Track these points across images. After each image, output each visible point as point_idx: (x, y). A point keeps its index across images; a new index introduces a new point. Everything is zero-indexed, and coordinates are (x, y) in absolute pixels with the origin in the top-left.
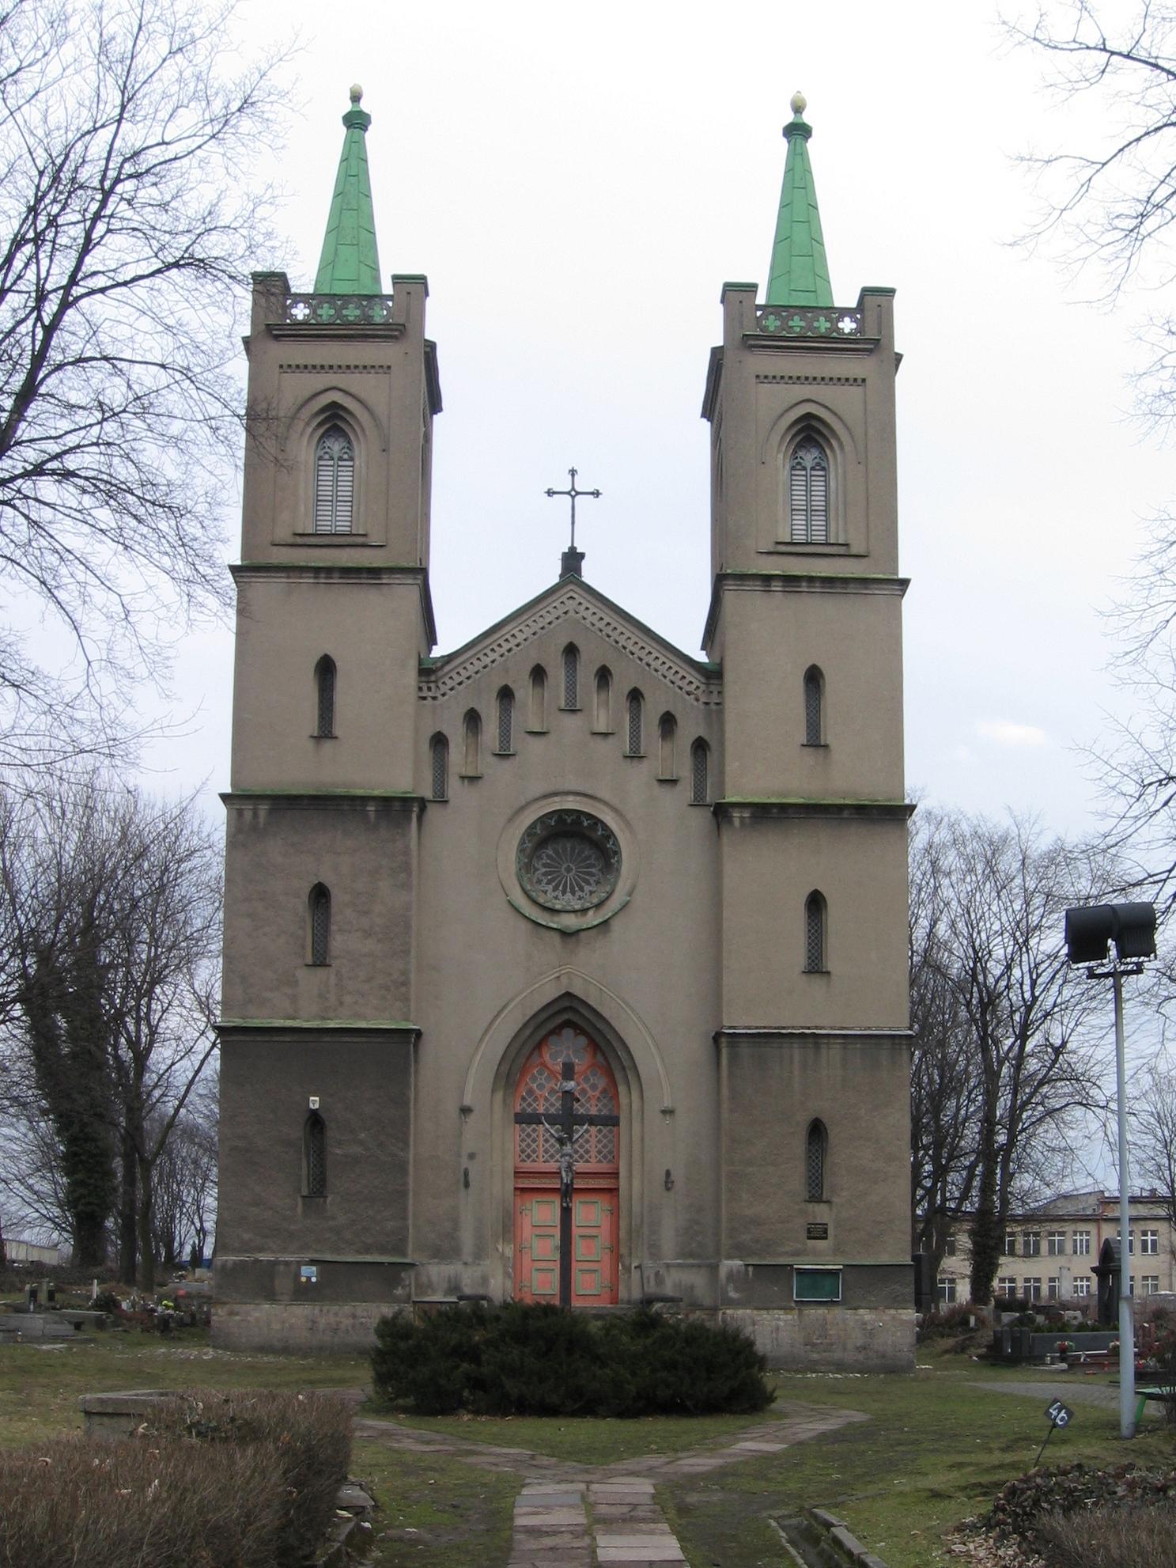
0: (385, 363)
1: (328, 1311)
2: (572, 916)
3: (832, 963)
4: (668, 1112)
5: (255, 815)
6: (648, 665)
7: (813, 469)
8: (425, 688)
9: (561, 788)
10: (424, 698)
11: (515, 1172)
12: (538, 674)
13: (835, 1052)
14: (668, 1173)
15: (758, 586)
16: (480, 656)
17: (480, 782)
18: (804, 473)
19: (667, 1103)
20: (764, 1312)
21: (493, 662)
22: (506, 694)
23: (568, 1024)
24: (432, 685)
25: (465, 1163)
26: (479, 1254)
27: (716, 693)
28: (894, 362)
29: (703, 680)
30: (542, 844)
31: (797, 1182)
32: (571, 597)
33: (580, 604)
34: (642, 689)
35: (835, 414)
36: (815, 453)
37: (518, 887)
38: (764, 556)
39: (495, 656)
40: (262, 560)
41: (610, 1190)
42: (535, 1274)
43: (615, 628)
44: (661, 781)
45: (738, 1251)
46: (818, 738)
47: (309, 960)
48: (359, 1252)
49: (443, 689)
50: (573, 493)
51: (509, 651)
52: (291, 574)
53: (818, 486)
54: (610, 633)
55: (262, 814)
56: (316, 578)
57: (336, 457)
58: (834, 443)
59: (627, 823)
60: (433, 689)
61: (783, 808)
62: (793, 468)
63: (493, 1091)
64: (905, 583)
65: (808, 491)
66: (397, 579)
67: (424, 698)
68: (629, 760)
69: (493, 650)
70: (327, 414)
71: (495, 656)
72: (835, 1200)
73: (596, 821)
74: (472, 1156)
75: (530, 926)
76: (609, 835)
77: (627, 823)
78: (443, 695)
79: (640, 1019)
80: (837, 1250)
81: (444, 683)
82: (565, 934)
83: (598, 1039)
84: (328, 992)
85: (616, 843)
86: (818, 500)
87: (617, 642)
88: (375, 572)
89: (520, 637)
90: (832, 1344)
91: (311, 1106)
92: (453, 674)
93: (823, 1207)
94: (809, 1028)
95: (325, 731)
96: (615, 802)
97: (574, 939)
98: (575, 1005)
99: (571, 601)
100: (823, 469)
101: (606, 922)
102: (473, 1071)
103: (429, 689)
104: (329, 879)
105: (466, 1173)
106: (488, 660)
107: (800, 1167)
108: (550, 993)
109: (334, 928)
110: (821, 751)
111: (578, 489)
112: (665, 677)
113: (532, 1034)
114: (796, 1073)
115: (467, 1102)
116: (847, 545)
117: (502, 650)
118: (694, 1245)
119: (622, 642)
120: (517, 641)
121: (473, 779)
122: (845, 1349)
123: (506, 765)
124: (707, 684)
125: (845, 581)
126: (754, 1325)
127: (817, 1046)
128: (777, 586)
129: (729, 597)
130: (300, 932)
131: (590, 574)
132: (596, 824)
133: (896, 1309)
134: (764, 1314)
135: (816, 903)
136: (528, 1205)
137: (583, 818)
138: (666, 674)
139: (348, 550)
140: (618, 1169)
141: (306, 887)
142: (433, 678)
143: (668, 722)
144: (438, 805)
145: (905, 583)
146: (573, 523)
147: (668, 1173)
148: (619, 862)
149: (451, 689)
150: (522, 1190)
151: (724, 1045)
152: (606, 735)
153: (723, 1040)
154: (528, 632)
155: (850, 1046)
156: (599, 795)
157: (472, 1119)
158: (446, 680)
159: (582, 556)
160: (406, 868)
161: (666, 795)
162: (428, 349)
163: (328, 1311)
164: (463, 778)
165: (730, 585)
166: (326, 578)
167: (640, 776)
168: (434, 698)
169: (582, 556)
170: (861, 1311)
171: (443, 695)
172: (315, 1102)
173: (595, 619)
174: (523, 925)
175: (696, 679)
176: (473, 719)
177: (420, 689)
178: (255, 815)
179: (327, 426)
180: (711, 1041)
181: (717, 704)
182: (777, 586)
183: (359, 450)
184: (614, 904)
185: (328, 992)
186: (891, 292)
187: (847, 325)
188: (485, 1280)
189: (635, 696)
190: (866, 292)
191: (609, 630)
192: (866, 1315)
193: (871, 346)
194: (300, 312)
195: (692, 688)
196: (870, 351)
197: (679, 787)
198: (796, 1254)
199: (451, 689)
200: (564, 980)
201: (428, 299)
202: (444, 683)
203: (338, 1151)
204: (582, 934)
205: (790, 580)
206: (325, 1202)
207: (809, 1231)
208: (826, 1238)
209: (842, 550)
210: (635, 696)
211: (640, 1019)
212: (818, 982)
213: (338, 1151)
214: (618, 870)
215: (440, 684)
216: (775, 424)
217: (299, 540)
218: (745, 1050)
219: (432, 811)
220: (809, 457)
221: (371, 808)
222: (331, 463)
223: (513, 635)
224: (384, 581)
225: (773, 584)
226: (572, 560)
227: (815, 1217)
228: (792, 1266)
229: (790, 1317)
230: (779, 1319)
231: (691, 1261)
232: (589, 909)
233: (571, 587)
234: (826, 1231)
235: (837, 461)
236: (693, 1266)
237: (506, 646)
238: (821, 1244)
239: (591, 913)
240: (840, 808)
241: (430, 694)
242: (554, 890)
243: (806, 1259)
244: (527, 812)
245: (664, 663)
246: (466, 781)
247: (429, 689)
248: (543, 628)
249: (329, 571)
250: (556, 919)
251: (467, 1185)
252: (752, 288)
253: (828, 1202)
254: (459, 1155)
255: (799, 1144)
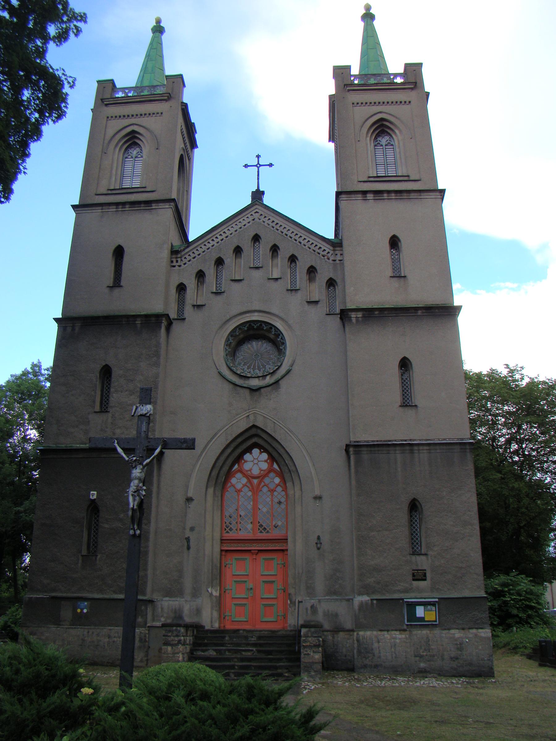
0: (160, 112)
1: (93, 633)
2: (257, 380)
3: (418, 399)
4: (318, 498)
5: (73, 329)
6: (300, 243)
7: (386, 145)
8: (175, 261)
9: (250, 309)
10: (174, 266)
11: (221, 540)
12: (238, 251)
13: (424, 455)
14: (319, 538)
15: (360, 196)
16: (206, 243)
17: (204, 308)
18: (381, 147)
19: (317, 493)
20: (386, 633)
21: (213, 246)
22: (219, 262)
23: (256, 445)
24: (179, 260)
25: (188, 534)
26: (196, 594)
27: (339, 255)
28: (425, 96)
29: (331, 248)
30: (241, 343)
31: (404, 542)
32: (257, 212)
33: (261, 215)
34: (296, 255)
35: (396, 118)
36: (387, 138)
37: (225, 366)
38: (362, 183)
39: (214, 243)
40: (90, 202)
41: (283, 550)
42: (233, 607)
43: (281, 226)
44: (308, 302)
45: (366, 589)
46: (400, 271)
47: (97, 408)
48: (115, 592)
49: (185, 261)
50: (258, 166)
51: (222, 240)
52: (104, 207)
53: (390, 153)
54: (278, 228)
55: (77, 329)
56: (116, 208)
57: (134, 156)
58: (397, 131)
59: (289, 326)
60: (179, 261)
61: (382, 310)
62: (375, 146)
63: (207, 488)
64: (443, 192)
65: (385, 156)
66: (161, 205)
67: (174, 266)
68: (290, 292)
69: (213, 240)
70: (130, 143)
71: (214, 243)
72: (430, 553)
73: (272, 326)
74: (192, 529)
75: (231, 386)
76: (278, 333)
77: (289, 326)
78: (185, 264)
79: (299, 440)
80: (433, 588)
81: (185, 258)
82: (254, 391)
83: (274, 454)
84: (107, 428)
85: (283, 338)
86: (391, 159)
87: (282, 233)
88: (148, 203)
89: (228, 233)
90: (434, 656)
91: (91, 497)
92: (191, 253)
93: (423, 558)
94: (406, 441)
95: (117, 283)
96: (281, 315)
97: (257, 393)
98: (259, 432)
99: (257, 214)
100: (392, 145)
101: (277, 382)
102: (194, 475)
103: (177, 261)
104: (111, 362)
105: (188, 539)
106: (210, 245)
107: (405, 531)
108: (243, 426)
109: (112, 390)
110: (402, 279)
111: (260, 168)
112: (310, 248)
113: (233, 451)
114: (399, 470)
115: (190, 495)
116: (408, 176)
117: (218, 240)
118: (337, 586)
119: (285, 231)
120: (226, 235)
121: (199, 307)
122: (443, 659)
123: (219, 298)
124: (334, 250)
125: (409, 192)
126: (379, 642)
127: (412, 452)
128: (370, 196)
129: (342, 204)
130: (93, 393)
131: (267, 200)
132: (271, 328)
133: (477, 628)
134: (386, 635)
135: (405, 364)
136: (230, 562)
137: (263, 325)
138: (310, 247)
139: (135, 195)
140: (287, 536)
141: (98, 367)
142: (179, 256)
143: (312, 271)
144: (179, 321)
145: (443, 192)
146: (258, 179)
147: (319, 538)
148: (285, 348)
149: (189, 261)
150: (227, 551)
151: (351, 453)
152: (276, 279)
153: (351, 449)
154: (232, 230)
155: (433, 451)
156: (272, 311)
157: (192, 505)
158: (187, 256)
159: (263, 193)
160: (157, 354)
161: (312, 309)
162: (184, 107)
163: (93, 633)
164: (194, 306)
165: (343, 197)
166: (122, 208)
167: (296, 300)
168: (180, 266)
169: (263, 193)
170: (452, 631)
171: (185, 264)
172: (94, 495)
173: (270, 222)
174: (227, 387)
175: (328, 248)
176: (200, 275)
177: (172, 262)
178: (73, 329)
179: (130, 143)
180: (344, 452)
181: (340, 260)
182: (370, 196)
183: (145, 151)
184: (282, 371)
185: (107, 428)
186: (421, 65)
187: (399, 80)
188: (198, 611)
189: (293, 259)
190: (407, 66)
191: (278, 227)
192: (457, 634)
193: (412, 86)
194: (120, 95)
195: (325, 253)
196: (412, 89)
197: (319, 305)
198: (406, 591)
199: (189, 261)
200: (252, 417)
201: (185, 89)
202: (185, 258)
203: (106, 526)
204: (262, 390)
205: (378, 193)
206: (96, 559)
207: (413, 575)
208: (425, 580)
209: (406, 178)
210: (293, 259)
211: (299, 440)
212: (410, 412)
213: (106, 526)
214: (284, 353)
215: (183, 259)
216: (363, 125)
217: (110, 192)
218: (365, 456)
219: (176, 326)
220: (384, 140)
221: (138, 322)
222: (132, 159)
223: (224, 232)
224: (153, 207)
225: (368, 195)
226: (258, 195)
227: (417, 565)
228: (403, 599)
229: (403, 636)
230: (395, 638)
231: (335, 597)
232: (267, 375)
233: (257, 206)
234: (425, 575)
235: (398, 138)
236: (337, 599)
237: (220, 238)
238: (422, 584)
239: (268, 377)
240: (416, 309)
241: (178, 264)
242: (248, 369)
243: (413, 595)
244: (231, 323)
245: (309, 241)
246: (196, 307)
247: (177, 261)
248: (241, 228)
249: (124, 204)
250: (247, 382)
251: (189, 548)
252: (348, 68)
253: (426, 554)
254: (184, 529)
255: (403, 516)
